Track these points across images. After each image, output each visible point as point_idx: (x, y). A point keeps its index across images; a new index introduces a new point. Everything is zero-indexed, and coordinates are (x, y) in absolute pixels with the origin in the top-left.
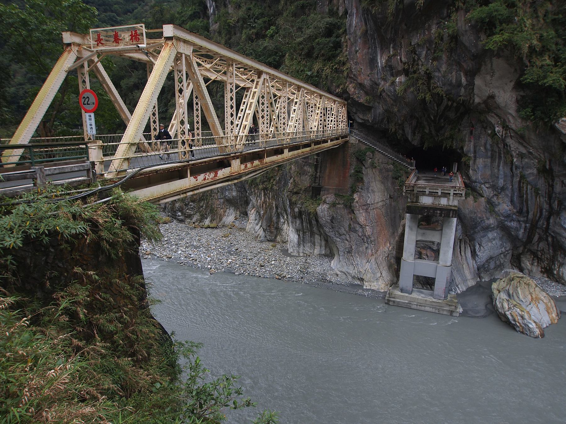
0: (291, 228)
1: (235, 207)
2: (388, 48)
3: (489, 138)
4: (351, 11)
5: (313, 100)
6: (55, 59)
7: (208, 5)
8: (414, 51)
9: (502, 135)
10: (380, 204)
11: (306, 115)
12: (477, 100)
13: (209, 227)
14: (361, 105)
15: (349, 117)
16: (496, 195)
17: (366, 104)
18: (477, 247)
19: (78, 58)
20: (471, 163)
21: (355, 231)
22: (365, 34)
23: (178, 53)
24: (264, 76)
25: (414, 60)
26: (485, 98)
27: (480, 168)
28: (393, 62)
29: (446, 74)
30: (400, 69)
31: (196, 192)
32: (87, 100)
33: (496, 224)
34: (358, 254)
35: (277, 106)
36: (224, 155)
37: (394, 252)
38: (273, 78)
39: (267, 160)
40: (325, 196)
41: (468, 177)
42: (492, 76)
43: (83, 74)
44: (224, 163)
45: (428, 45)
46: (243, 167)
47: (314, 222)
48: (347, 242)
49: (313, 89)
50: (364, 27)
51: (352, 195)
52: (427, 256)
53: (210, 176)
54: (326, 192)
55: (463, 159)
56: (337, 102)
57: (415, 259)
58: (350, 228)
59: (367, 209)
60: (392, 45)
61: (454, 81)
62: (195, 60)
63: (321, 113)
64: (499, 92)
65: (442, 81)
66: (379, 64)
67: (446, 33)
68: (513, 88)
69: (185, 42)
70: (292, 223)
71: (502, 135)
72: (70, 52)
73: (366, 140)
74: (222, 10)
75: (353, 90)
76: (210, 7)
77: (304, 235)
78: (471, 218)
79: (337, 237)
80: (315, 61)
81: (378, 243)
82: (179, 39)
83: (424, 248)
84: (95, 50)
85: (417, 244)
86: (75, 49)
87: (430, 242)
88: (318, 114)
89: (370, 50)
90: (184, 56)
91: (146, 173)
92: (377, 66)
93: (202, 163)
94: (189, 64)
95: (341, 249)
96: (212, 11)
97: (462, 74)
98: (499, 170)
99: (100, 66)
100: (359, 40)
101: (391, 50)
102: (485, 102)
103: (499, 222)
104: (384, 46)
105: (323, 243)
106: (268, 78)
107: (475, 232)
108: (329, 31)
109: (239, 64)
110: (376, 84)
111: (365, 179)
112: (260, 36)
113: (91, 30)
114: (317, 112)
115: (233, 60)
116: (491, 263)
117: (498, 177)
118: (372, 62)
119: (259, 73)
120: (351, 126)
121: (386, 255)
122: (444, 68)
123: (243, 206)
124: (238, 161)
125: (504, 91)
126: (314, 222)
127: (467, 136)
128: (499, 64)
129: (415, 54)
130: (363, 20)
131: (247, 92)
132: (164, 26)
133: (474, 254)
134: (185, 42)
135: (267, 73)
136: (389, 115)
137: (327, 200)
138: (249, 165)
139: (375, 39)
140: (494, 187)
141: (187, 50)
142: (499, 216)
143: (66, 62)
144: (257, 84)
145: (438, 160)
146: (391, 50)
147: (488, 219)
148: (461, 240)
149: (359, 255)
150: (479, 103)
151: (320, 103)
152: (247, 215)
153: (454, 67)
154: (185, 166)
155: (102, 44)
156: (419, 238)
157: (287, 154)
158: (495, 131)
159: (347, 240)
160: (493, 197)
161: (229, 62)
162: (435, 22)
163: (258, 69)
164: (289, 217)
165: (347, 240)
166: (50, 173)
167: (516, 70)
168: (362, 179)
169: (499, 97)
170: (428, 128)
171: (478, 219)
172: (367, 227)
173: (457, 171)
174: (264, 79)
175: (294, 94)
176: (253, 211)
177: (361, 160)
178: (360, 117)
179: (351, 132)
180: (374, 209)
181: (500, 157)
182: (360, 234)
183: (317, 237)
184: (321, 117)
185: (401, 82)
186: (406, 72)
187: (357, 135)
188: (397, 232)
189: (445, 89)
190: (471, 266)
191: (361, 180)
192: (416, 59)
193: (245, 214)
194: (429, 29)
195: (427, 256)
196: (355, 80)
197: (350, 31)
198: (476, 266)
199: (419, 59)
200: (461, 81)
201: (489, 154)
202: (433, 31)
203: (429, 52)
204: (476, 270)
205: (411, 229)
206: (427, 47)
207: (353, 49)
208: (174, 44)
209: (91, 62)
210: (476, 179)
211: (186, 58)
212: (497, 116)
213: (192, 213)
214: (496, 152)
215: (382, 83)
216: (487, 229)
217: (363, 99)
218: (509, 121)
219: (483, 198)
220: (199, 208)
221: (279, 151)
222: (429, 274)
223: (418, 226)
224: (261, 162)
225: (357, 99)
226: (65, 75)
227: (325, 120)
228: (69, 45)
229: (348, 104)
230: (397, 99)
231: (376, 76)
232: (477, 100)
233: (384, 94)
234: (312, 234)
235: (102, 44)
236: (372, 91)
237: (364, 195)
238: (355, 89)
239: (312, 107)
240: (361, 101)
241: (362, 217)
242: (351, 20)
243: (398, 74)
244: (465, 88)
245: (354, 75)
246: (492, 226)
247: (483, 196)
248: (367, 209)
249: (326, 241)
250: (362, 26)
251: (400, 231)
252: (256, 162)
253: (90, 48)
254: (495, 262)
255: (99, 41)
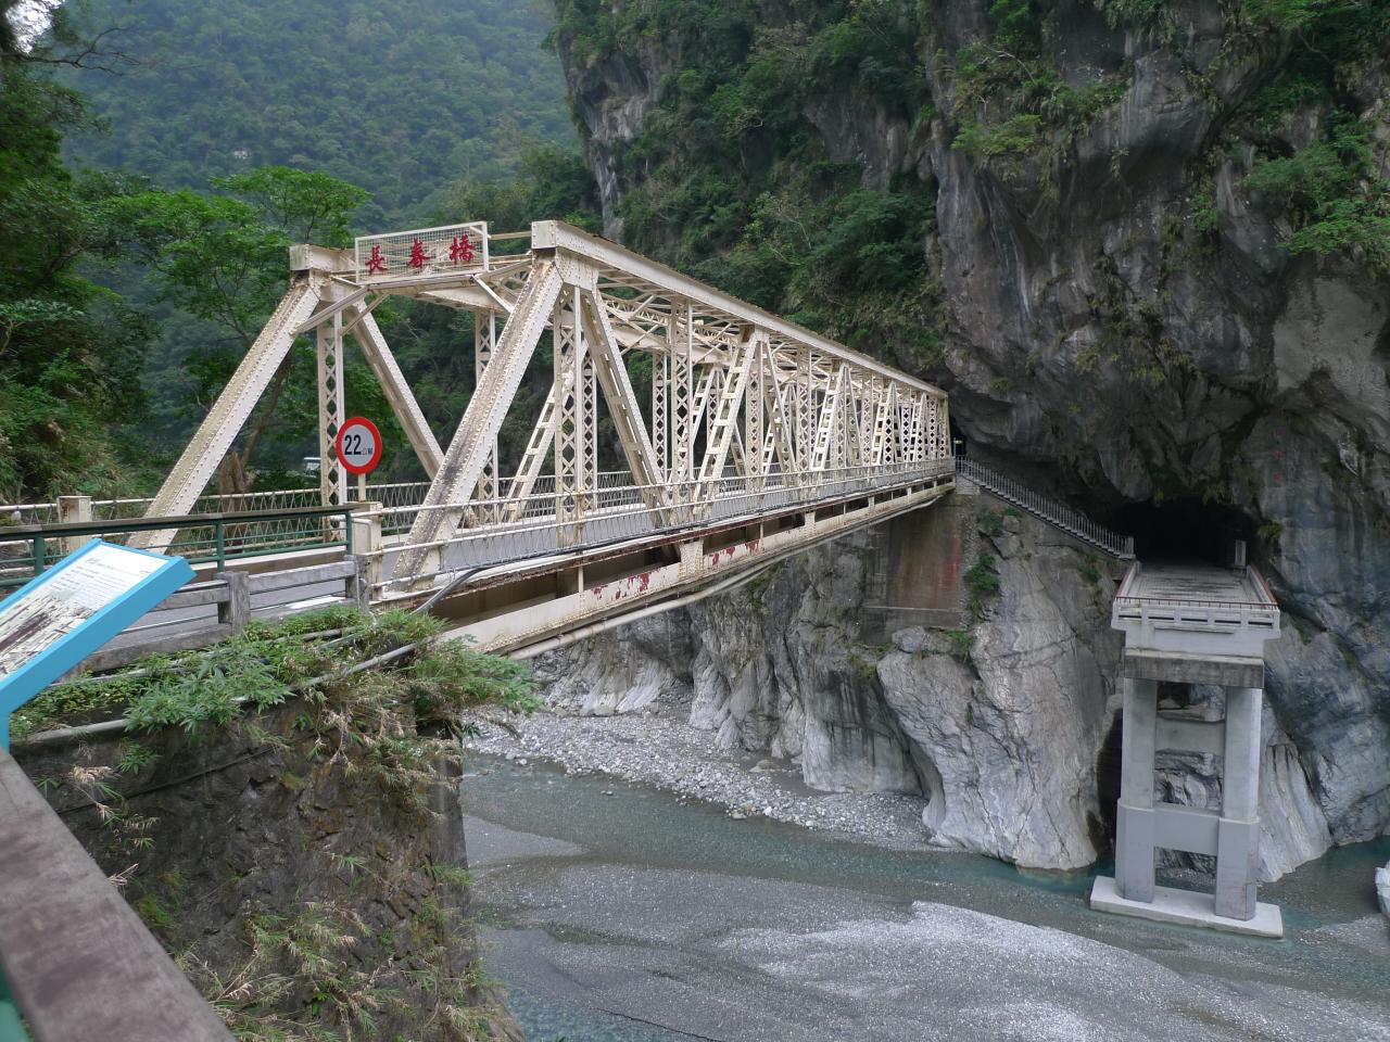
0: (809, 719)
1: (661, 660)
2: (1044, 262)
3: (1325, 475)
4: (948, 181)
5: (872, 393)
6: (271, 305)
7: (600, 180)
8: (1112, 269)
9: (1360, 469)
10: (1048, 652)
11: (841, 427)
12: (1284, 383)
13: (594, 715)
14: (984, 400)
15: (955, 432)
16: (1359, 625)
17: (995, 397)
18: (1322, 767)
19: (322, 305)
20: (1283, 540)
21: (983, 726)
22: (984, 233)
23: (566, 286)
24: (756, 337)
25: (1113, 290)
26: (1304, 377)
27: (1310, 552)
28: (1059, 295)
29: (1198, 321)
30: (1079, 311)
31: (597, 629)
32: (354, 443)
33: (1368, 703)
34: (996, 789)
35: (697, 395)
36: (664, 533)
37: (1095, 784)
38: (777, 339)
39: (768, 542)
40: (900, 633)
41: (1279, 578)
42: (1317, 323)
43: (329, 341)
44: (662, 555)
45: (1145, 254)
46: (709, 560)
47: (871, 702)
48: (962, 756)
49: (867, 363)
50: (981, 216)
51: (970, 628)
52: (1188, 794)
53: (629, 588)
54: (901, 621)
55: (1262, 533)
56: (924, 396)
57: (1155, 804)
58: (969, 719)
59: (1012, 667)
60: (1054, 256)
61: (1220, 338)
62: (602, 308)
63: (888, 422)
64: (1340, 360)
65: (1189, 338)
66: (1026, 302)
67: (1189, 222)
68: (1376, 350)
69: (582, 259)
70: (813, 702)
71: (1360, 469)
72: (304, 289)
73: (1001, 486)
74: (633, 190)
75: (961, 363)
76: (605, 182)
77: (845, 737)
78: (1298, 687)
79: (936, 743)
80: (865, 293)
81: (1049, 758)
82: (568, 254)
83: (1176, 771)
84: (362, 284)
85: (1157, 761)
86: (315, 283)
87: (1193, 755)
88: (880, 424)
89: (1000, 269)
90: (577, 293)
91: (483, 583)
92: (1019, 306)
93: (612, 553)
94: (589, 313)
95: (948, 775)
96: (608, 192)
97: (1238, 319)
98: (1360, 558)
99: (370, 322)
100: (971, 247)
101: (1054, 266)
102: (1307, 386)
103: (1376, 698)
104: (1035, 258)
105: (899, 759)
106: (767, 340)
107: (1312, 727)
108: (893, 228)
109: (700, 308)
110: (1019, 348)
111: (1005, 589)
112: (728, 237)
113: (357, 239)
114: (878, 419)
115: (687, 301)
116: (1365, 812)
117: (1359, 578)
118: (1008, 297)
119: (746, 330)
120: (959, 451)
121: (1074, 793)
122: (1190, 307)
123: (682, 659)
124: (698, 546)
125: (1352, 358)
126: (871, 702)
127: (1266, 472)
128: (1333, 293)
129: (1115, 273)
130: (978, 200)
131: (707, 374)
132: (534, 224)
133: (1314, 785)
134: (582, 259)
135: (764, 330)
136: (1056, 422)
137: (905, 642)
138: (724, 557)
139: (1010, 244)
140: (1349, 604)
141: (586, 280)
142: (1374, 681)
143: (296, 312)
144: (741, 355)
145: (1194, 534)
146: (1054, 266)
147: (1345, 689)
148: (1274, 749)
149: (998, 792)
150: (1290, 391)
151: (888, 398)
152: (692, 682)
153: (1218, 303)
154: (573, 562)
155: (381, 269)
156: (1164, 745)
157: (812, 527)
158: (1339, 458)
159: (964, 752)
160: (1351, 630)
161: (666, 303)
162: (1159, 198)
163: (743, 321)
164: (805, 688)
165: (964, 752)
166: (261, 588)
167: (1377, 306)
168: (996, 586)
169: (1340, 371)
170: (1160, 454)
171: (1318, 691)
172: (1017, 715)
173: (1248, 563)
174: (759, 342)
175: (824, 377)
176: (707, 672)
177: (991, 537)
178: (982, 430)
179: (958, 466)
180: (1031, 666)
181: (1359, 526)
182: (999, 735)
183: (881, 742)
184: (889, 431)
185: (1083, 343)
186: (1094, 317)
187: (977, 474)
188: (1100, 730)
189: (1198, 355)
190: (1312, 821)
191: (995, 590)
192: (1119, 286)
193: (688, 681)
194: (1146, 215)
195: (1188, 794)
196: (964, 339)
197: (947, 226)
198: (1323, 823)
199: (1126, 286)
200: (1237, 335)
201: (1330, 516)
202: (1157, 219)
203: (1149, 269)
204: (1327, 831)
205: (1138, 718)
206: (1144, 258)
207: (957, 266)
208: (558, 263)
209: (350, 313)
210: (1301, 583)
211: (583, 298)
212: (1340, 419)
213: (551, 677)
214: (1346, 511)
215: (1035, 345)
216: (1345, 716)
217: (983, 384)
218: (1375, 433)
219: (1325, 635)
220: (569, 665)
221: (793, 520)
222: (1198, 845)
223: (1158, 715)
224: (752, 547)
225: (972, 386)
226: (290, 345)
227: (897, 440)
228: (303, 274)
229: (950, 399)
230: (1075, 382)
231: (1019, 330)
232: (1284, 383)
233: (1041, 373)
234: (869, 734)
235: (381, 269)
236: (1017, 371)
237: (1004, 628)
238: (965, 361)
239: (906, 416)
240: (984, 389)
241: (1000, 689)
242: (948, 203)
243: (1076, 322)
244: (1251, 355)
245: (963, 329)
246: (1358, 709)
247: (1324, 630)
248: (1012, 667)
249: (907, 753)
250: (975, 213)
251: (1107, 724)
252: (741, 550)
253: (353, 280)
254: (1376, 809)
255: (374, 264)
